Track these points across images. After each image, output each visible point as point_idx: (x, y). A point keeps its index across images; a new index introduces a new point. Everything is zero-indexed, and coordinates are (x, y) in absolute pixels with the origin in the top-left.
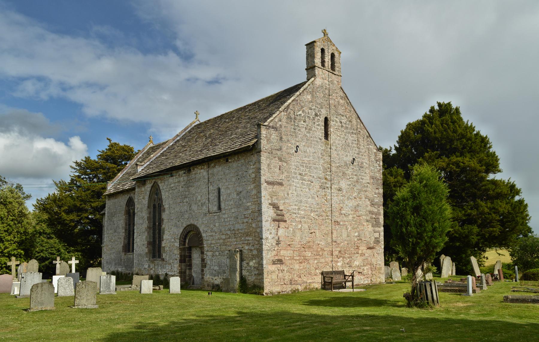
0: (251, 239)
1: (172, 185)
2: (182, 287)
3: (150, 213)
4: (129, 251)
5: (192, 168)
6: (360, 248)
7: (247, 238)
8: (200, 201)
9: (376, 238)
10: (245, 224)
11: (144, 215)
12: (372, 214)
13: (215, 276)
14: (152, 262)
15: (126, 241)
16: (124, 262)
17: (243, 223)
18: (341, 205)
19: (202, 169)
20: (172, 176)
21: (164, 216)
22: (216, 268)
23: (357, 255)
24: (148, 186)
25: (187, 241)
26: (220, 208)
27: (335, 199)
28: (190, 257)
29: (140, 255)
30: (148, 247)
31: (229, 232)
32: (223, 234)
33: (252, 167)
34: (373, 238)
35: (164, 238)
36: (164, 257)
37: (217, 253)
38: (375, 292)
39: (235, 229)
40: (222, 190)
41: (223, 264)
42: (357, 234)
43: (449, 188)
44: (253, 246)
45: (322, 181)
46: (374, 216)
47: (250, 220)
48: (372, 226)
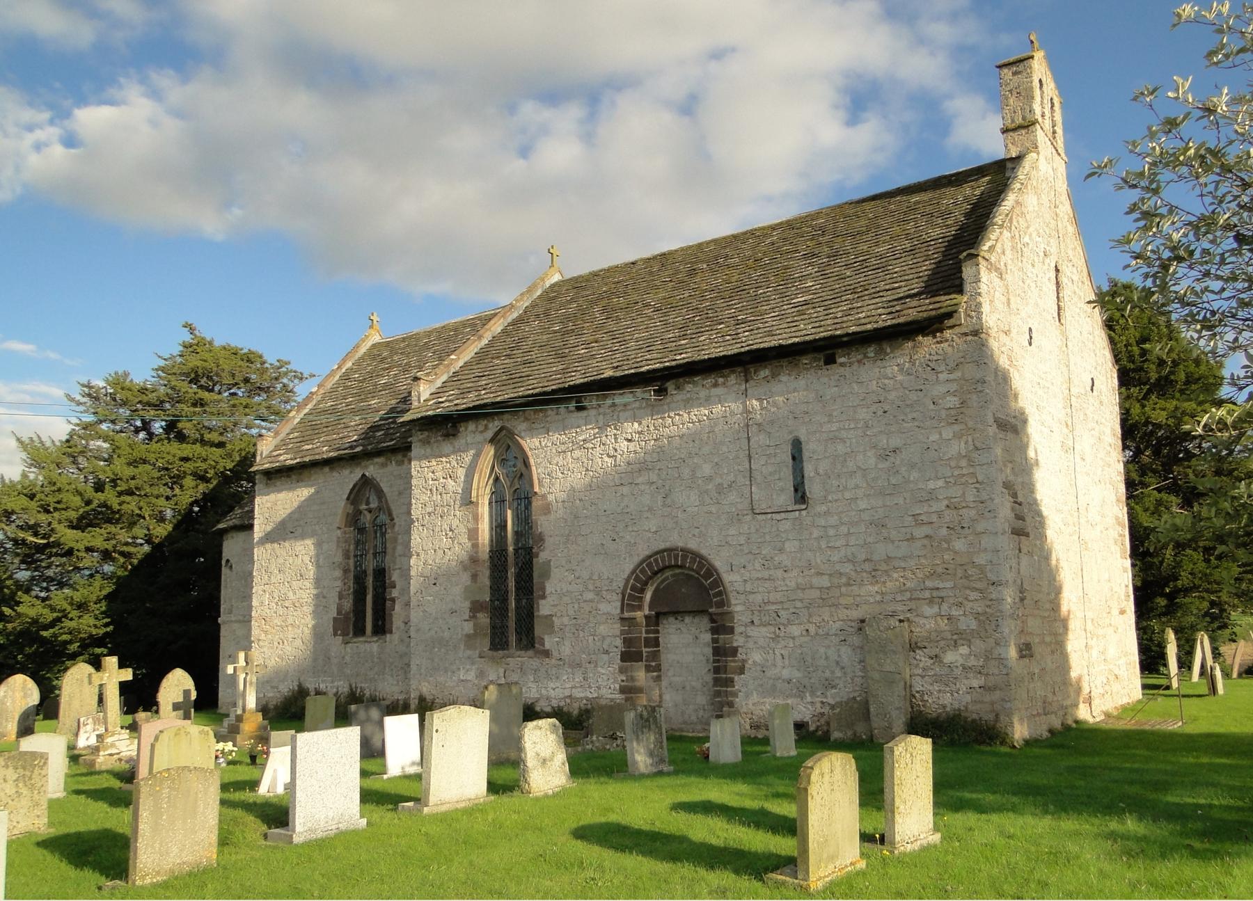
0: (949, 584)
2: (578, 768)
4: (359, 631)
5: (670, 386)
8: (710, 479)
10: (918, 544)
15: (348, 604)
17: (912, 539)
20: (580, 409)
26: (800, 495)
31: (847, 568)
32: (820, 574)
35: (549, 588)
39: (876, 557)
47: (944, 531)
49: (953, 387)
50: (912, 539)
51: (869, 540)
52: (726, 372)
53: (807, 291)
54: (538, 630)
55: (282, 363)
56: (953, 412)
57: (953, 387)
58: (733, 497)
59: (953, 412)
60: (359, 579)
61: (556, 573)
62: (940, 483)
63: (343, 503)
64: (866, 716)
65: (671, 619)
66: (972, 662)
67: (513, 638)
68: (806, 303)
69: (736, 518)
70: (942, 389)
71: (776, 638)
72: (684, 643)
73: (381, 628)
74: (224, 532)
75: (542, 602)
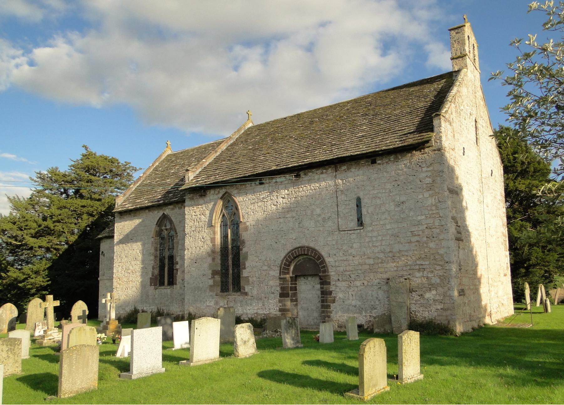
0: (427, 263)
2: (260, 345)
4: (162, 284)
5: (302, 173)
8: (320, 215)
10: (413, 244)
15: (157, 272)
17: (410, 242)
20: (261, 184)
26: (360, 223)
28: (295, 289)
31: (381, 255)
32: (369, 258)
35: (247, 264)
39: (394, 250)
43: (48, 277)
47: (425, 239)
49: (429, 174)
50: (410, 242)
51: (391, 243)
52: (327, 167)
53: (363, 131)
54: (242, 283)
55: (127, 163)
56: (429, 185)
57: (429, 174)
58: (330, 223)
59: (429, 185)
60: (162, 260)
61: (250, 258)
62: (423, 217)
63: (154, 226)
64: (390, 322)
65: (302, 278)
66: (438, 297)
67: (231, 287)
68: (363, 136)
69: (331, 233)
70: (424, 175)
71: (349, 287)
72: (308, 289)
73: (172, 282)
74: (101, 239)
75: (244, 271)
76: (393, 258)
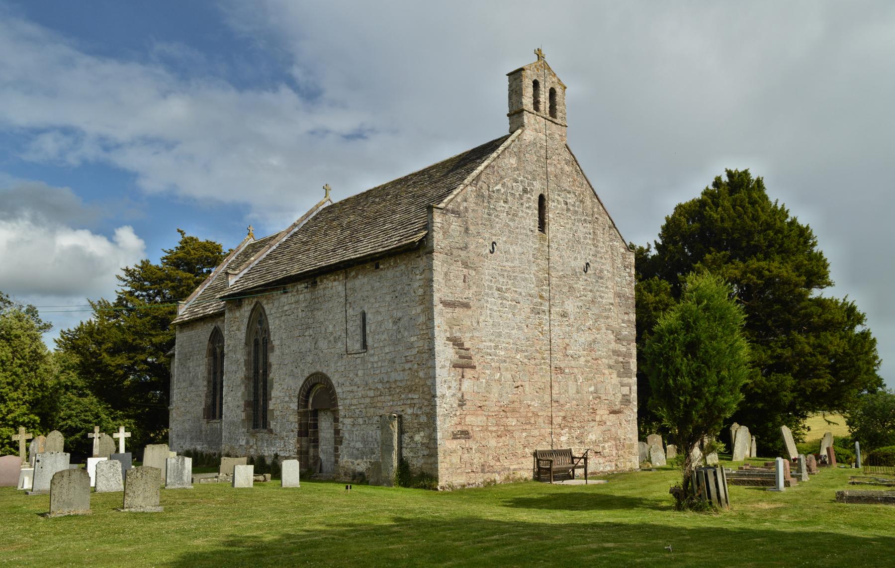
0: (417, 396)
1: (286, 308)
2: (303, 477)
3: (249, 354)
5: (318, 280)
6: (598, 412)
7: (410, 396)
8: (332, 333)
9: (624, 395)
10: (407, 373)
11: (239, 356)
12: (618, 355)
13: (357, 458)
14: (253, 435)
15: (210, 401)
16: (206, 435)
17: (404, 370)
18: (567, 341)
19: (335, 280)
20: (285, 293)
21: (273, 358)
22: (359, 445)
23: (592, 424)
24: (246, 309)
25: (311, 400)
26: (364, 346)
27: (556, 330)
28: (316, 426)
29: (233, 423)
30: (245, 410)
31: (380, 386)
32: (370, 389)
33: (418, 277)
34: (619, 396)
35: (273, 395)
36: (272, 427)
37: (361, 421)
38: (622, 486)
39: (391, 380)
40: (369, 316)
41: (370, 439)
42: (592, 389)
44: (421, 408)
45: (535, 300)
46: (621, 359)
47: (416, 366)
48: (618, 376)
76: (483, 471)
